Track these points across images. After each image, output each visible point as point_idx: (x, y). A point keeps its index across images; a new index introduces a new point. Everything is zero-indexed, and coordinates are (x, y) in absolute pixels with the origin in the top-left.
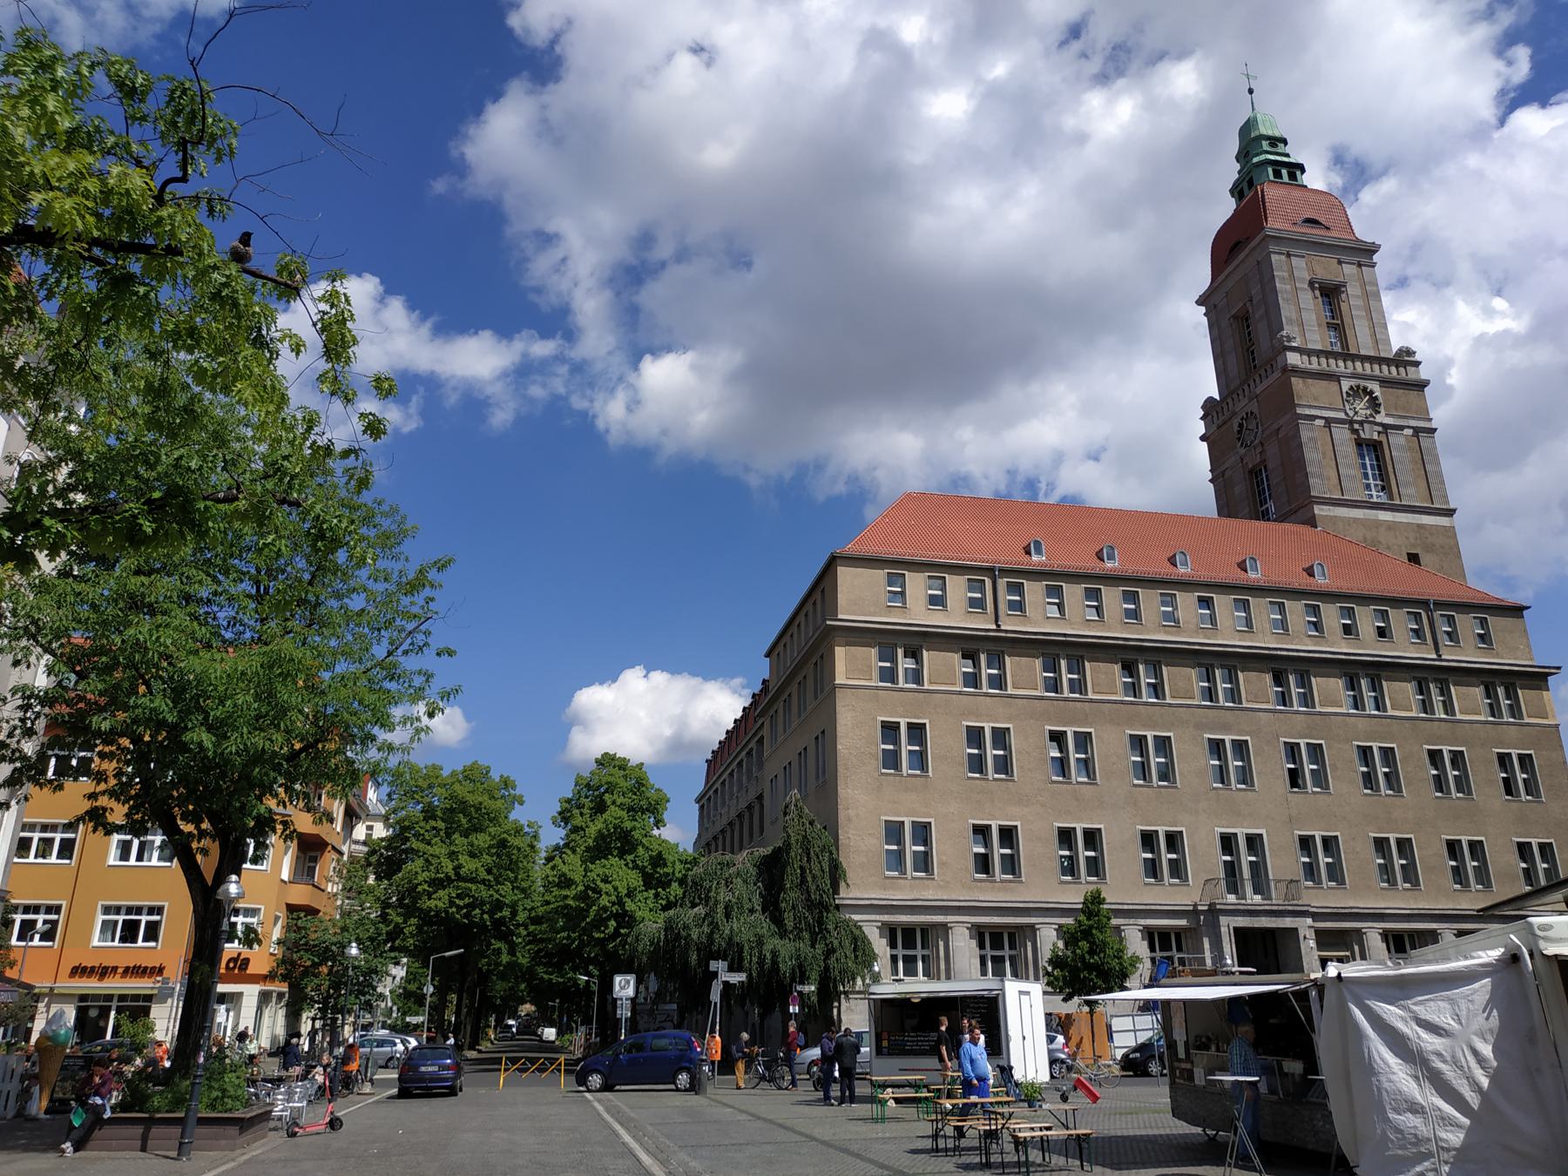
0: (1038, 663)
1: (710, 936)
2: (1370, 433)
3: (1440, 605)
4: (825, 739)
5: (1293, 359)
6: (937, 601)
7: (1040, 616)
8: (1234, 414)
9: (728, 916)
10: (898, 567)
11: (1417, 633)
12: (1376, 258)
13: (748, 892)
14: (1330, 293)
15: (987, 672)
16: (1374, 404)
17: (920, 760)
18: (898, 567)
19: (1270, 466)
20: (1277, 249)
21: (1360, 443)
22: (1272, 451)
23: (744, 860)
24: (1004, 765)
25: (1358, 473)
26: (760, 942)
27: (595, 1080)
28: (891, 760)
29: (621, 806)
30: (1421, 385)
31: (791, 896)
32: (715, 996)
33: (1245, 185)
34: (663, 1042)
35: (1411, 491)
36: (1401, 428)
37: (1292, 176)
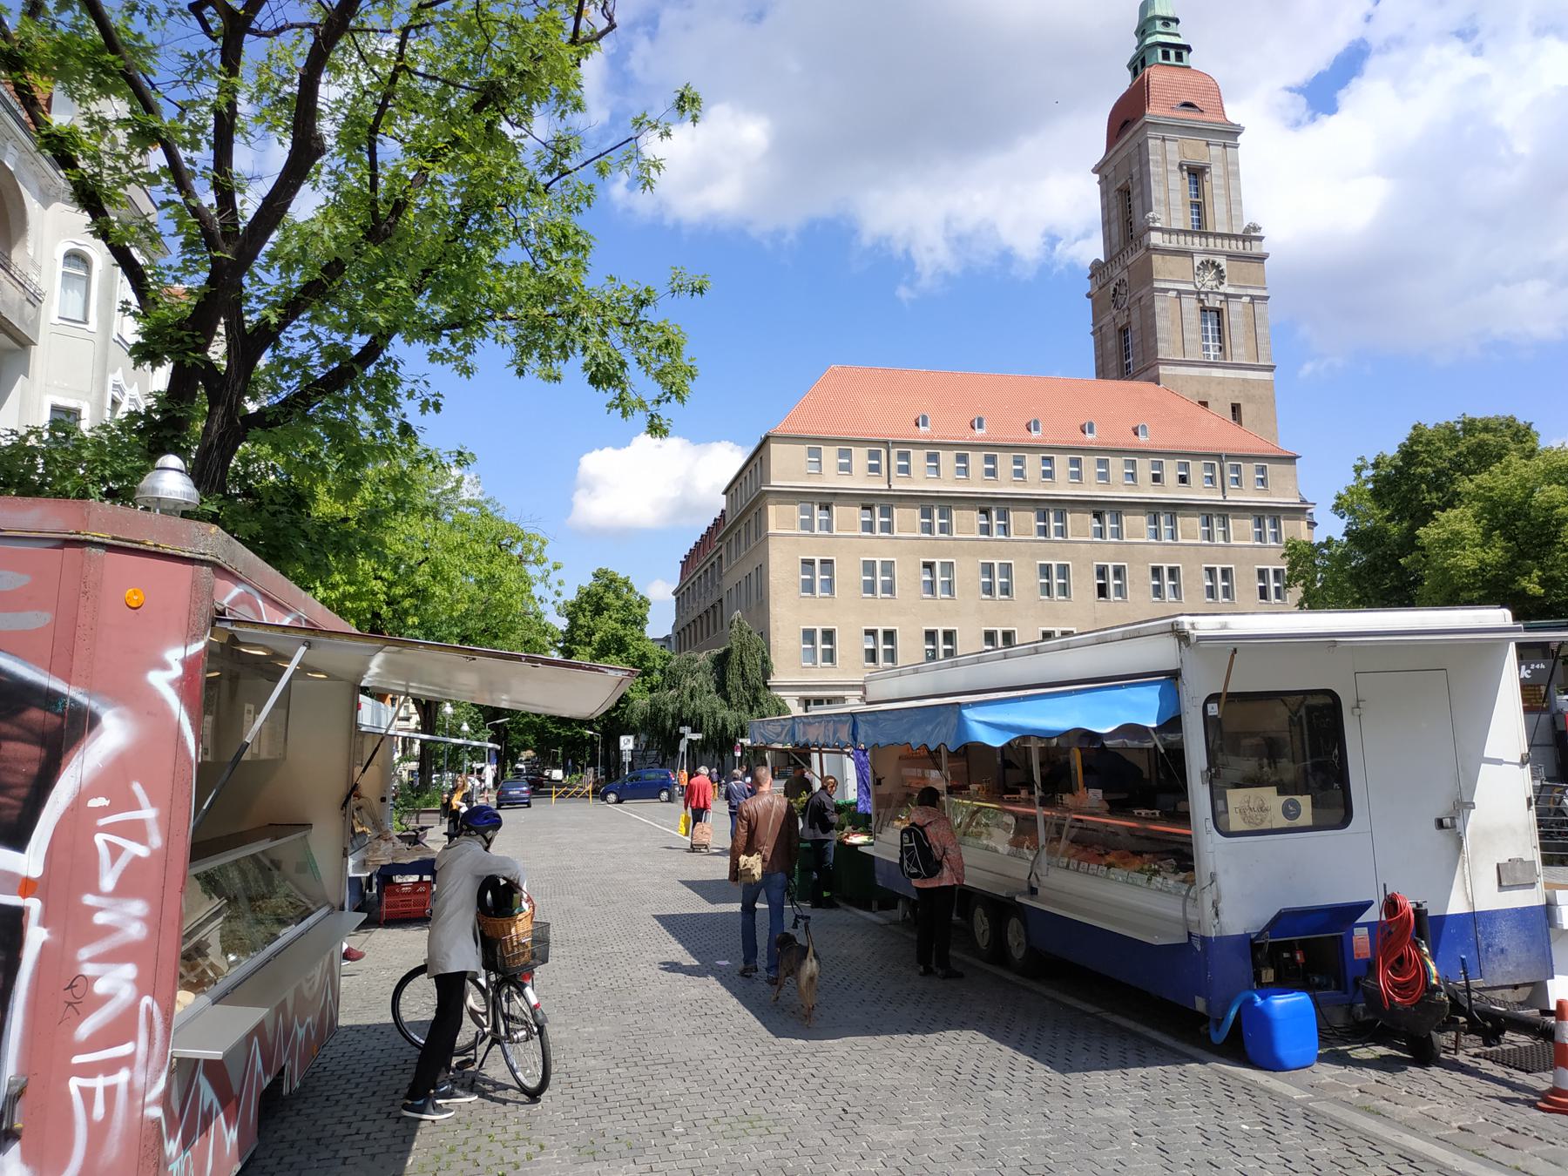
0: (918, 512)
1: (680, 709)
3: (1229, 457)
4: (761, 570)
5: (1156, 239)
6: (846, 468)
7: (920, 480)
8: (1111, 279)
9: (692, 697)
10: (815, 442)
11: (1211, 479)
12: (1240, 139)
13: (703, 680)
14: (1196, 173)
15: (879, 520)
16: (1220, 275)
17: (829, 585)
18: (815, 442)
20: (1154, 134)
22: (1135, 316)
23: (704, 658)
24: (889, 588)
25: (1197, 336)
26: (714, 713)
27: (612, 797)
28: (809, 586)
29: (616, 620)
30: (1261, 258)
31: (734, 680)
32: (683, 747)
34: (652, 776)
35: (1242, 351)
36: (1240, 296)
37: (1179, 57)
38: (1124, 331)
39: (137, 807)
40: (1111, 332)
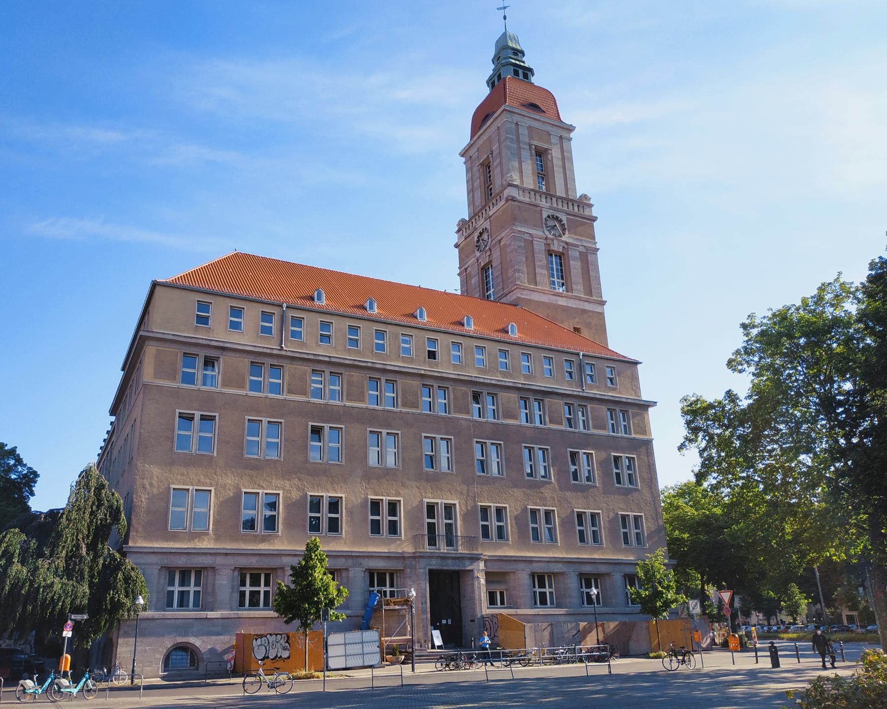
2: (556, 247)
8: (475, 229)
19: (494, 265)
21: (550, 253)
22: (496, 254)
33: (496, 78)
36: (577, 246)
38: (485, 269)
39: (189, 591)
40: (474, 270)
